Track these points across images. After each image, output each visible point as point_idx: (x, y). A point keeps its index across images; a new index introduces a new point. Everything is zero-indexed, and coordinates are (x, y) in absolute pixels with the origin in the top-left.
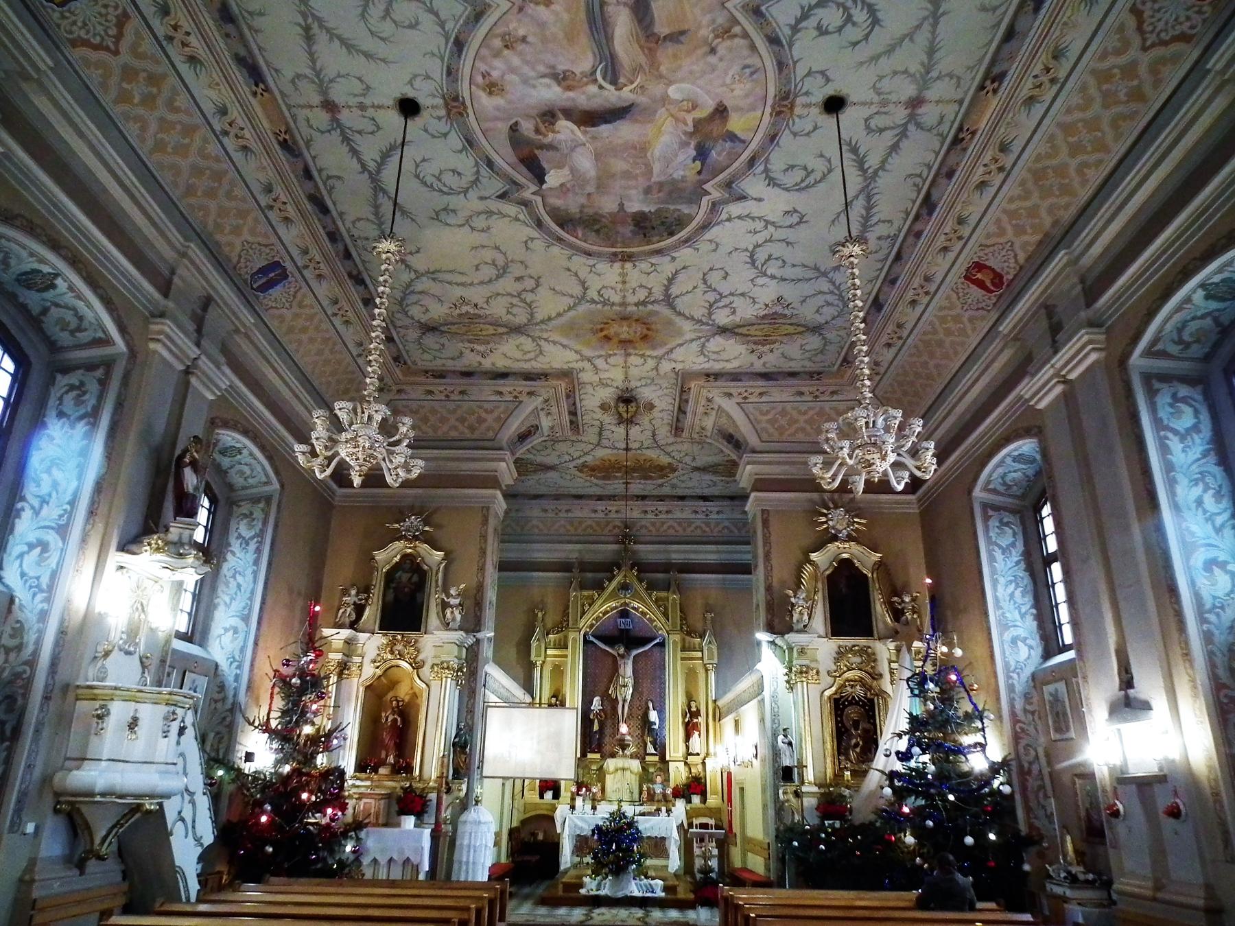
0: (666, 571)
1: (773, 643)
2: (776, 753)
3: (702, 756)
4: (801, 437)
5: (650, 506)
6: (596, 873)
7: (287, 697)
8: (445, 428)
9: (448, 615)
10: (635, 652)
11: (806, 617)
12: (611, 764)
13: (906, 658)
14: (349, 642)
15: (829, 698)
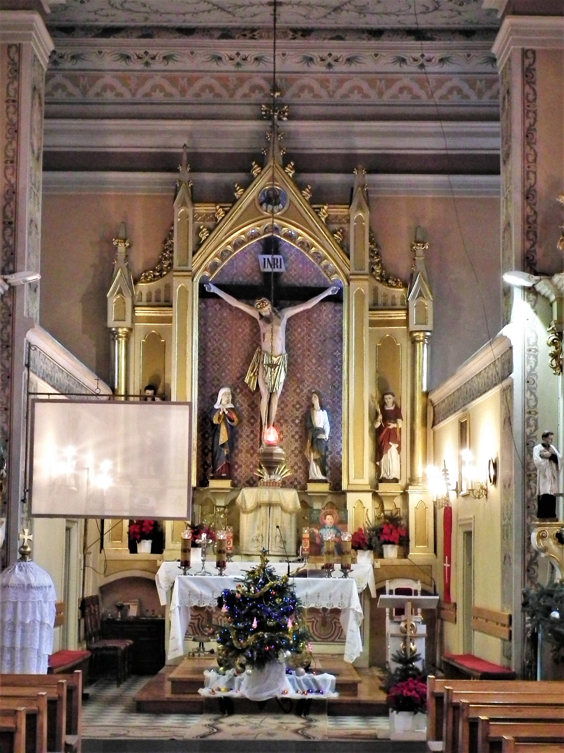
0: (349, 171)
1: (530, 291)
3: (402, 483)
6: (225, 663)
10: (290, 312)
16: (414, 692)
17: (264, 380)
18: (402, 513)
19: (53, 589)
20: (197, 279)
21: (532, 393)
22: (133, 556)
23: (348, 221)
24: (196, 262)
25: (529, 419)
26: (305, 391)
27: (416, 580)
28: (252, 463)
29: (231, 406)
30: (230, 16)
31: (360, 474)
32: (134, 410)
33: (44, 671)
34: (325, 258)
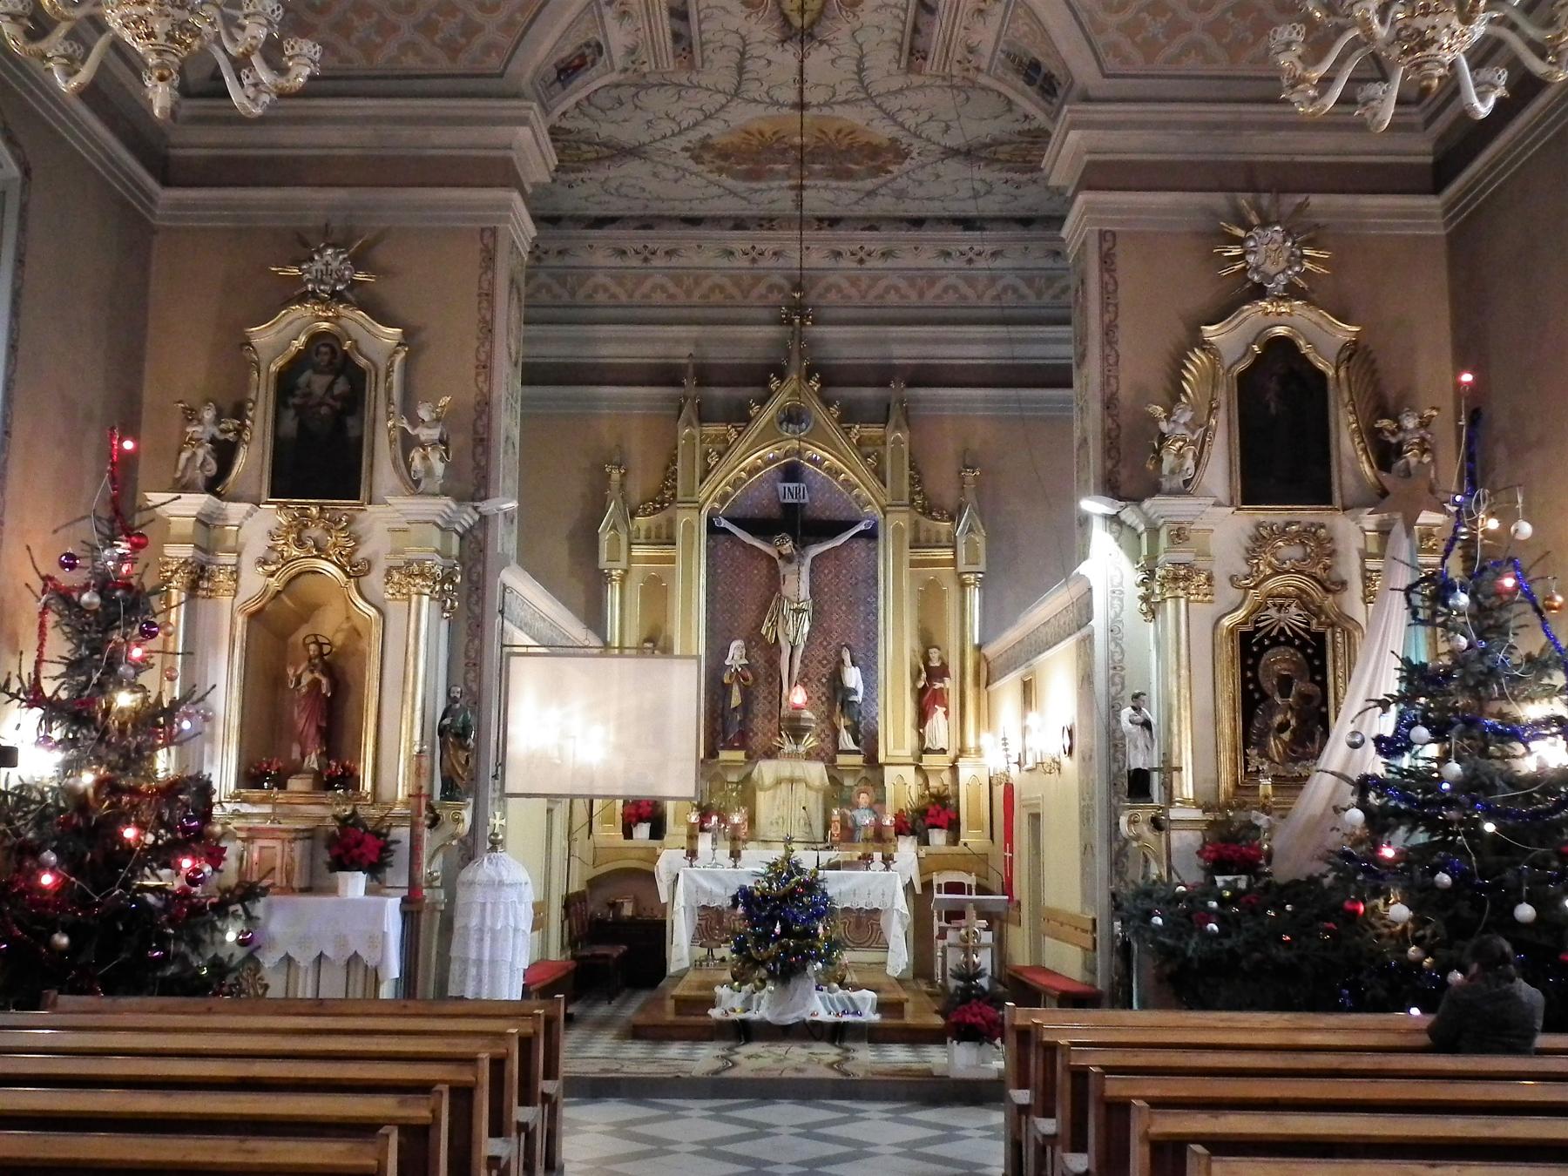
0: (884, 384)
1: (1114, 519)
2: (1115, 743)
3: (951, 754)
4: (1191, 64)
5: (845, 237)
6: (740, 977)
7: (76, 634)
8: (392, 48)
9: (417, 463)
10: (816, 550)
11: (1189, 463)
12: (767, 770)
13: (1402, 546)
14: (205, 522)
15: (1231, 631)
16: (979, 1018)
17: (784, 630)
18: (950, 791)
19: (530, 886)
20: (705, 512)
21: (1117, 645)
22: (629, 843)
23: (884, 443)
24: (703, 493)
25: (1113, 675)
26: (833, 644)
27: (969, 873)
28: (770, 730)
29: (745, 662)
30: (744, 203)
31: (899, 744)
32: (629, 665)
33: (517, 995)
34: (857, 486)
